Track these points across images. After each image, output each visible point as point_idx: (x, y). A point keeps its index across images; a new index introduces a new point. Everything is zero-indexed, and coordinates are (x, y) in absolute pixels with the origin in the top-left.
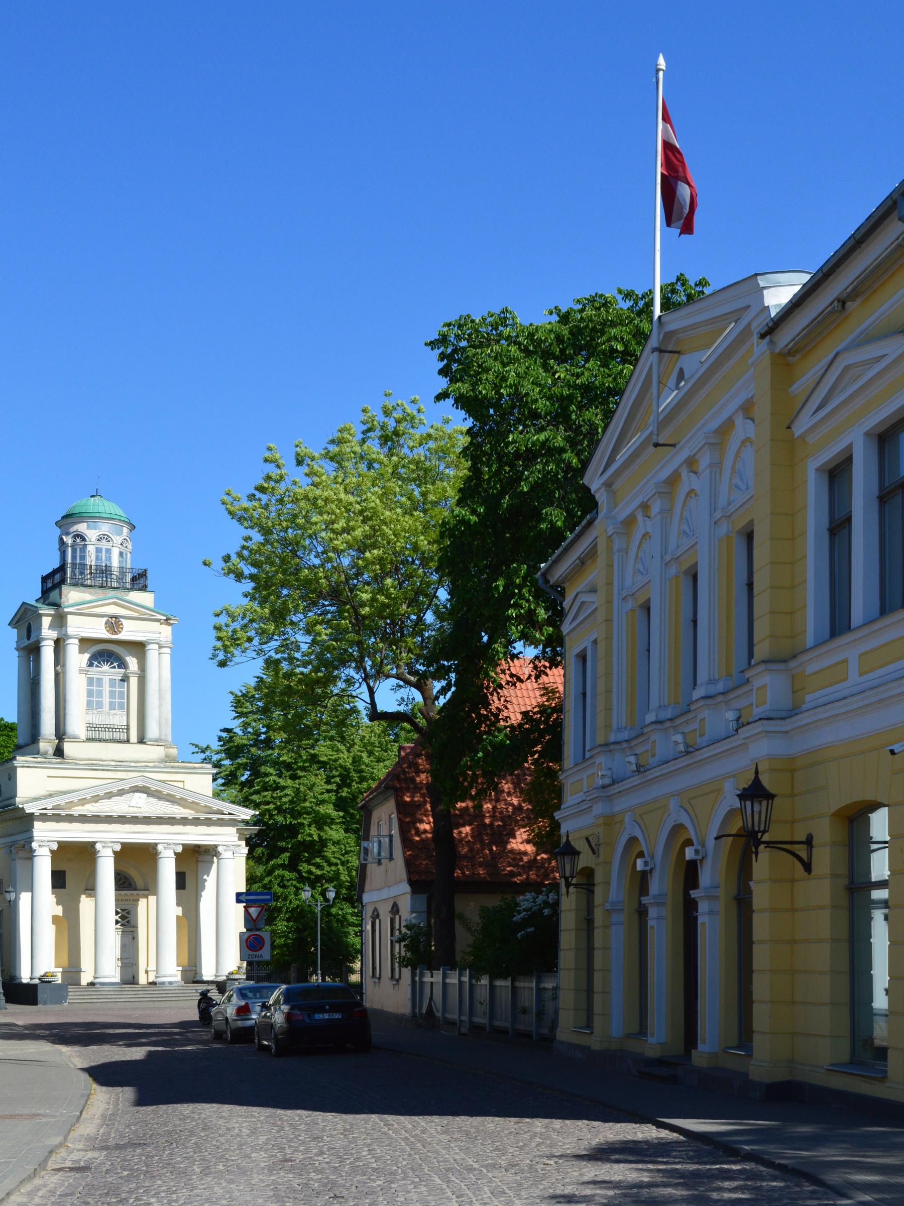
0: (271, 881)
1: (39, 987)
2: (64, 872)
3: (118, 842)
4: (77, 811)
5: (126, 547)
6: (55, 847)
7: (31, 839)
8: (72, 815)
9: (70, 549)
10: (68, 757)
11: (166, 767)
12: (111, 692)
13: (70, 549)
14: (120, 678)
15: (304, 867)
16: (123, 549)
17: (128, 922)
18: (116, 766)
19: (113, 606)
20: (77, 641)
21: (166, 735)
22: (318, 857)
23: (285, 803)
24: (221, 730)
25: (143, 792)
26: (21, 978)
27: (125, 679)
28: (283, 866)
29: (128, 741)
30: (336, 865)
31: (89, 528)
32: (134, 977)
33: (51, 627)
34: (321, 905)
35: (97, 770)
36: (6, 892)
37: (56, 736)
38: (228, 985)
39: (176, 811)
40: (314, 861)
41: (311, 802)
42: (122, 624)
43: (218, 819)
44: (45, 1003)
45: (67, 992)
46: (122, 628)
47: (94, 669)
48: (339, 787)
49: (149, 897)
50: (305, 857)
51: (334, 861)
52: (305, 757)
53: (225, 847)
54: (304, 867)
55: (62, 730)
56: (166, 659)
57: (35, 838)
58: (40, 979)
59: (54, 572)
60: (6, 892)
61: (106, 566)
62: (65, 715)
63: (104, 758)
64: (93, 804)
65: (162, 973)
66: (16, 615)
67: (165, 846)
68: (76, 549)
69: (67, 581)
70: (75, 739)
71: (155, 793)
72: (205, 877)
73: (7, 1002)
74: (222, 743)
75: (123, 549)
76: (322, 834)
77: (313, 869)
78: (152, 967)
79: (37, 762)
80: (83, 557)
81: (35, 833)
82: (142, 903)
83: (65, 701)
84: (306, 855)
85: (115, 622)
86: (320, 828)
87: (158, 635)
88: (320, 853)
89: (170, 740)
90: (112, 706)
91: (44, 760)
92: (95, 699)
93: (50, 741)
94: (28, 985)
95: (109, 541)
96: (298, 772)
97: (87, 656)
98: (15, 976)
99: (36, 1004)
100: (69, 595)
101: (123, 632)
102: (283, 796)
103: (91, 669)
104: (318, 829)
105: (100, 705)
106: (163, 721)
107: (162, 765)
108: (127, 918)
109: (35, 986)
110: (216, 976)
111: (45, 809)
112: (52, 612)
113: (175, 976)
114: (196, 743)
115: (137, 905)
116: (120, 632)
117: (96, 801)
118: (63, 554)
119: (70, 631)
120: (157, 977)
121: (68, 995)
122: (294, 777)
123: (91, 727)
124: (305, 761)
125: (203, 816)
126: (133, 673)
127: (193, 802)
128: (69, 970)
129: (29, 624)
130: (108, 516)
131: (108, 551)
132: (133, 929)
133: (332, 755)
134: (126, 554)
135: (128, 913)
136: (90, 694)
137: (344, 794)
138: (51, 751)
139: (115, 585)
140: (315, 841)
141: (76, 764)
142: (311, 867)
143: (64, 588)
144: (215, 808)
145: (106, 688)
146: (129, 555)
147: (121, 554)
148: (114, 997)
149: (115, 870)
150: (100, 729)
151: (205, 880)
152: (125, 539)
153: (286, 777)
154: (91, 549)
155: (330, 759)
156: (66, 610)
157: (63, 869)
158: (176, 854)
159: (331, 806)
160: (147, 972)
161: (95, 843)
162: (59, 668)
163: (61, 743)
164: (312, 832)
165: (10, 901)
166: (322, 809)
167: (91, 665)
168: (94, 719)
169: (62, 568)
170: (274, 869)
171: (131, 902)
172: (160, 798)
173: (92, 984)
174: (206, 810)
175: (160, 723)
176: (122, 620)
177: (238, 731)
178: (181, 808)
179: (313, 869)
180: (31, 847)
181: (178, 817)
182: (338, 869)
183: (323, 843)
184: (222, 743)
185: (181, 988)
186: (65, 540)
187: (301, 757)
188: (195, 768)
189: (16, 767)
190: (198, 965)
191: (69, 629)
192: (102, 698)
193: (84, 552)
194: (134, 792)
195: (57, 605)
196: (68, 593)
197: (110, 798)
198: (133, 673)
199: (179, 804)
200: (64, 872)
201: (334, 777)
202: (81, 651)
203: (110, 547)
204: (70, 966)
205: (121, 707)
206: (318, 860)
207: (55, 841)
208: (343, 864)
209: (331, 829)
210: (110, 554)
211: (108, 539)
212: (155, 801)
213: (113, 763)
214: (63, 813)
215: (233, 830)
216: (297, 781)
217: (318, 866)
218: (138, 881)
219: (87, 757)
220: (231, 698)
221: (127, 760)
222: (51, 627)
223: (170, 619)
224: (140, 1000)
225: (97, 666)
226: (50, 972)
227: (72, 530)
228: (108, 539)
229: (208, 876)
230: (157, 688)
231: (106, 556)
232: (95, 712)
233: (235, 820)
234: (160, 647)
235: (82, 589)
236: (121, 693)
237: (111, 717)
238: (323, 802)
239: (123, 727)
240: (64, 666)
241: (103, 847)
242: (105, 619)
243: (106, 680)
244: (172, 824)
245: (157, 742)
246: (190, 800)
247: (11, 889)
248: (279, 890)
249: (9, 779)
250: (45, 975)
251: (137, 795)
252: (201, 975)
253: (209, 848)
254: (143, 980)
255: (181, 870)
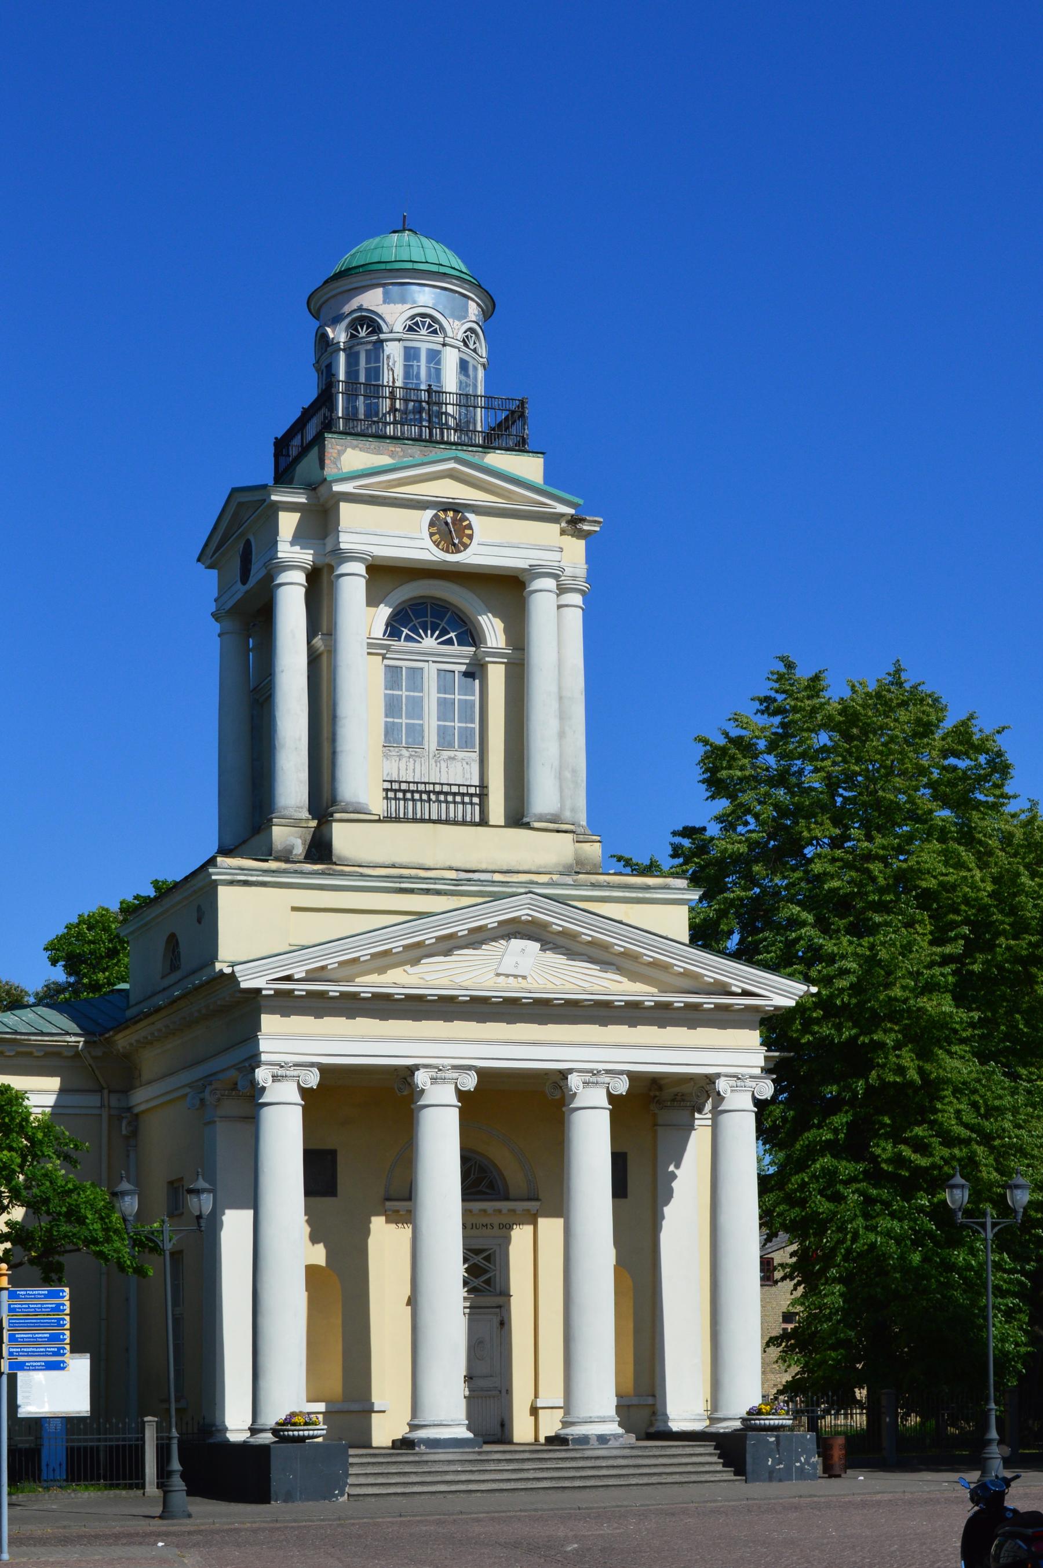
0: (803, 1185)
1: (273, 1453)
2: (333, 1153)
3: (470, 1068)
4: (368, 984)
5: (475, 350)
6: (313, 1079)
7: (254, 1060)
8: (354, 996)
9: (342, 356)
10: (339, 858)
11: (577, 885)
12: (442, 703)
13: (342, 356)
14: (463, 668)
15: (884, 1149)
16: (468, 355)
17: (488, 1282)
18: (457, 882)
19: (448, 481)
20: (360, 568)
21: (573, 810)
22: (920, 1124)
23: (841, 991)
24: (675, 834)
25: (530, 938)
26: (225, 1429)
27: (475, 672)
28: (831, 1147)
29: (484, 822)
30: (967, 1142)
31: (387, 299)
32: (502, 1425)
33: (299, 538)
34: (994, 1225)
35: (411, 891)
36: (191, 1191)
37: (310, 811)
38: (750, 1443)
39: (614, 987)
40: (907, 1135)
41: (904, 988)
42: (470, 527)
43: (718, 1007)
44: (288, 1498)
45: (347, 1465)
46: (471, 537)
47: (402, 644)
48: (972, 947)
49: (542, 1222)
50: (885, 1125)
51: (965, 1133)
52: (881, 881)
53: (733, 1082)
54: (884, 1149)
55: (326, 795)
56: (574, 619)
57: (264, 1057)
58: (275, 1432)
59: (307, 415)
60: (191, 1191)
61: (429, 391)
62: (334, 753)
63: (429, 863)
64: (408, 967)
65: (426, 1417)
66: (215, 529)
67: (588, 1077)
68: (357, 354)
69: (337, 425)
70: (359, 814)
71: (561, 941)
72: (672, 1168)
73: (189, 1493)
74: (681, 860)
75: (468, 355)
76: (928, 1067)
77: (907, 1152)
78: (552, 1394)
79: (266, 872)
80: (375, 373)
81: (264, 1045)
82: (520, 1236)
83: (334, 718)
84: (887, 1120)
85: (454, 520)
86: (924, 1054)
87: (556, 556)
88: (924, 1113)
89: (584, 823)
90: (445, 740)
91: (283, 865)
92: (404, 721)
93: (296, 823)
94: (244, 1446)
95: (435, 332)
96: (870, 914)
97: (384, 612)
98: (214, 1425)
99: (269, 1503)
100: (344, 458)
101: (473, 548)
102: (834, 977)
103: (395, 644)
104: (919, 1056)
105: (416, 736)
106: (568, 774)
107: (569, 880)
108: (485, 1271)
109: (265, 1449)
110: (713, 1420)
111: (288, 978)
112: (302, 500)
113: (603, 1421)
114: (627, 856)
115: (508, 1240)
116: (466, 546)
117: (415, 962)
118: (327, 374)
119: (347, 541)
120: (565, 1424)
121: (347, 1475)
122: (860, 929)
123: (395, 790)
124: (882, 891)
125: (678, 1000)
126: (494, 655)
127: (655, 964)
128: (346, 1407)
129: (248, 543)
130: (435, 268)
131: (434, 357)
132: (499, 1300)
133: (946, 875)
134: (475, 369)
135: (488, 1259)
136: (392, 707)
137: (976, 968)
138: (299, 849)
139: (453, 437)
140: (911, 1083)
141: (362, 875)
142: (902, 1147)
143: (332, 444)
144: (710, 976)
145: (431, 695)
146: (481, 373)
147: (463, 365)
148: (463, 1477)
149: (463, 1149)
150: (417, 796)
151: (674, 1177)
152: (471, 330)
153: (838, 931)
154: (393, 351)
155: (942, 884)
156: (337, 488)
157: (329, 1146)
158: (612, 1098)
159: (948, 997)
160: (534, 1411)
161: (412, 1070)
162: (318, 641)
163: (324, 828)
164: (906, 1063)
165: (199, 1217)
166: (929, 1004)
167: (393, 629)
168: (403, 772)
169: (326, 398)
170: (812, 1152)
171: (496, 1231)
172: (572, 954)
173: (404, 1444)
174: (686, 983)
175: (560, 778)
176: (470, 516)
177: (714, 830)
178: (625, 980)
179: (907, 1152)
180: (253, 1083)
181: (619, 1000)
182: (974, 1153)
183: (932, 1087)
184: (681, 860)
185: (627, 1452)
186: (331, 335)
187: (873, 879)
188: (648, 888)
189: (215, 884)
190: (658, 1393)
191: (343, 537)
192: (421, 717)
193: (377, 360)
194: (508, 936)
195: (316, 486)
196: (340, 453)
197: (447, 953)
198: (494, 655)
199: (620, 970)
200: (333, 1153)
201: (953, 925)
202: (372, 601)
203: (439, 347)
204: (347, 1397)
205: (466, 744)
206: (919, 1131)
207: (312, 1065)
208: (986, 1139)
209: (950, 1054)
210: (439, 363)
211: (435, 327)
212: (560, 960)
213: (452, 875)
214: (334, 989)
215: (753, 1037)
216: (866, 941)
217: (921, 1147)
218: (514, 1176)
219: (388, 861)
220: (701, 750)
221: (483, 867)
222: (299, 538)
223: (582, 520)
224: (529, 1485)
225: (408, 638)
226: (301, 1413)
227: (347, 309)
228: (435, 327)
229: (677, 1166)
230: (554, 689)
231: (428, 368)
232: (405, 752)
233: (756, 1009)
234: (562, 590)
235: (374, 444)
236: (467, 706)
237: (443, 765)
238: (930, 988)
239: (472, 790)
240: (331, 634)
241: (434, 1080)
242: (429, 514)
243: (430, 671)
244: (604, 1022)
245: (555, 824)
246: (650, 955)
247: (201, 1184)
248: (823, 1206)
249: (199, 921)
250: (289, 1421)
251: (516, 944)
252: (666, 1418)
253: (686, 1088)
254: (522, 1430)
255: (477, 1244)
